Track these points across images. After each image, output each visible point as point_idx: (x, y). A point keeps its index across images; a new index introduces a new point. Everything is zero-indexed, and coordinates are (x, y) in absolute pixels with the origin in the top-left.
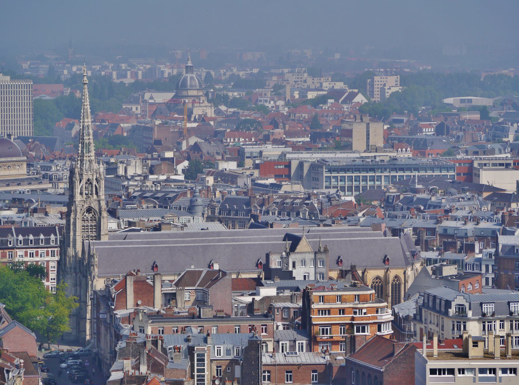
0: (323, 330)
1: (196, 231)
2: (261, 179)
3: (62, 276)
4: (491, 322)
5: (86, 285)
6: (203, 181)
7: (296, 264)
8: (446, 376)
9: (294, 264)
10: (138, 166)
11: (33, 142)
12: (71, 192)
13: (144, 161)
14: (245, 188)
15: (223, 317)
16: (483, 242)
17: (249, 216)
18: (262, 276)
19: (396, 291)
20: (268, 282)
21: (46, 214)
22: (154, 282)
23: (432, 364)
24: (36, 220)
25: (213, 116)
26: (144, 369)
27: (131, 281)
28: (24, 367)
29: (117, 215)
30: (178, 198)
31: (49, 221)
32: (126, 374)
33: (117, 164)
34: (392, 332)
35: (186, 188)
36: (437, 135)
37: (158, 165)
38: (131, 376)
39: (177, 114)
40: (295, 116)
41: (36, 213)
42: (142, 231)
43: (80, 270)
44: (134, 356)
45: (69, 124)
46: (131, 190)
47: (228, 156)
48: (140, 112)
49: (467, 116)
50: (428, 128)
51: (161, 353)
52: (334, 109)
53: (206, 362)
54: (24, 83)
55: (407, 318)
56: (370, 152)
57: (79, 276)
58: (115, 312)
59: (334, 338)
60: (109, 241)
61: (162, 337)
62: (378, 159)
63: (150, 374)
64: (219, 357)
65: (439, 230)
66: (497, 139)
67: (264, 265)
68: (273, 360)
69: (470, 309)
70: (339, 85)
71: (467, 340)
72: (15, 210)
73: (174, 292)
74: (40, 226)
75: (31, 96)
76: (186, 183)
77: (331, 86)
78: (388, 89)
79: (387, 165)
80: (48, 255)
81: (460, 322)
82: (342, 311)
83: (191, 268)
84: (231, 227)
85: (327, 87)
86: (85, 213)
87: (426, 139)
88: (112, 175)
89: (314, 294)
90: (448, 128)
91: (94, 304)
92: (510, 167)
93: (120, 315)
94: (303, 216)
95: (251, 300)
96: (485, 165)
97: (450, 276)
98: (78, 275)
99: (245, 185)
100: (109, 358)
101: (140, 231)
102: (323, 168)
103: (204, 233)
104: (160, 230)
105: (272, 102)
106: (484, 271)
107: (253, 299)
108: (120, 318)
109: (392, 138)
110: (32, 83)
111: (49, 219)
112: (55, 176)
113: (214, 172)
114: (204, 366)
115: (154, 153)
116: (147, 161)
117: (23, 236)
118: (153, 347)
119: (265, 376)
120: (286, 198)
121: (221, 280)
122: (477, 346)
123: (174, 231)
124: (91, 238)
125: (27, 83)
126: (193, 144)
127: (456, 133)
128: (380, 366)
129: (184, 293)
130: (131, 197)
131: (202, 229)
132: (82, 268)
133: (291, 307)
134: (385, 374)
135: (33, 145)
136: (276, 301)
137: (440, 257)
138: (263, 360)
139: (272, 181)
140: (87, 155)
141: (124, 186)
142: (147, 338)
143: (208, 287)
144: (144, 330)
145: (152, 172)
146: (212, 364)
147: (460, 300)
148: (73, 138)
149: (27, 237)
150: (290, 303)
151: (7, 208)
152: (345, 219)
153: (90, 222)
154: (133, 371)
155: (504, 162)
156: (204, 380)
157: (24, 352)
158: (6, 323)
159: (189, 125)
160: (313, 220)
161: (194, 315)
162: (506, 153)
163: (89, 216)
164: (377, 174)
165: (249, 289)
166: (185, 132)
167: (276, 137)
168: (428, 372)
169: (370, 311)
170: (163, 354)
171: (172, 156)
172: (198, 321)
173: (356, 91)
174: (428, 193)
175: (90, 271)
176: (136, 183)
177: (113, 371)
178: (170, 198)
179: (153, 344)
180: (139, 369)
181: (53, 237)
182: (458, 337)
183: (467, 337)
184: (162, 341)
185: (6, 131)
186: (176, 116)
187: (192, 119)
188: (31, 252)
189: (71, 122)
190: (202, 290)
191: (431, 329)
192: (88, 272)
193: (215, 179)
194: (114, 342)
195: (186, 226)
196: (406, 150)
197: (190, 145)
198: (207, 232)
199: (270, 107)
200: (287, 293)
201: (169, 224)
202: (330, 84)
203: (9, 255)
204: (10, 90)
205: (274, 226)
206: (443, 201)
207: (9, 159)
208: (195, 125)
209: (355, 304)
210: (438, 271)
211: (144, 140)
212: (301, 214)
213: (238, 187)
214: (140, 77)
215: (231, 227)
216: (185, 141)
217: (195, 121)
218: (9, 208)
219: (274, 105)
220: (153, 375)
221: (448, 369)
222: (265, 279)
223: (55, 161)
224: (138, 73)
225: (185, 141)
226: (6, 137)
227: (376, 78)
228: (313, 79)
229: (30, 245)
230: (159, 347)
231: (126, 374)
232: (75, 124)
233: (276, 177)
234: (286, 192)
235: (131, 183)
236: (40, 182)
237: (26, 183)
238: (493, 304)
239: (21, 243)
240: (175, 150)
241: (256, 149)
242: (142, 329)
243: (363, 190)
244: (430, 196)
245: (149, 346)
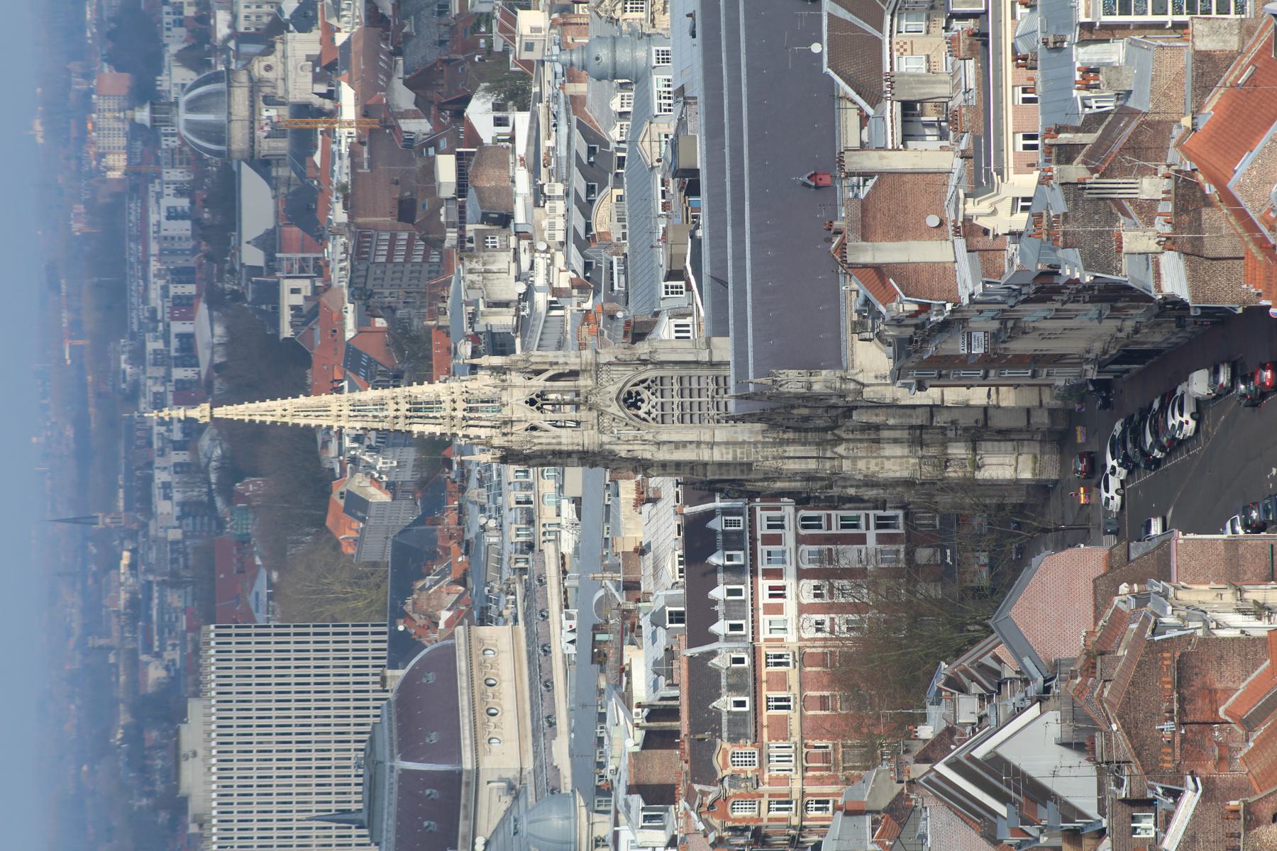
5: (877, 407)
6: (532, 44)
10: (484, 264)
12: (569, 460)
13: (469, 245)
21: (642, 551)
25: (316, 34)
26: (1151, 187)
27: (865, 250)
28: (1142, 581)
30: (591, 121)
31: (668, 541)
32: (1169, 243)
33: (477, 334)
35: (555, 97)
38: (1176, 227)
39: (312, 155)
41: (639, 583)
42: (699, 233)
43: (825, 430)
44: (1112, 218)
45: (347, 510)
46: (563, 281)
51: (1100, 132)
57: (847, 431)
58: (966, 301)
60: (731, 334)
63: (1169, 166)
72: (630, 653)
74: (681, 571)
76: (541, 101)
83: (821, 53)
86: (641, 413)
93: (974, 285)
98: (844, 436)
100: (1118, 323)
101: (700, 240)
110: (212, 627)
111: (660, 540)
112: (518, 536)
115: (442, 219)
116: (469, 234)
117: (716, 620)
118: (1080, 158)
123: (697, 126)
124: (721, 391)
125: (213, 643)
126: (412, 95)
130: (587, 278)
131: (694, 36)
141: (551, 306)
144: (1024, 199)
145: (505, 220)
148: (394, 499)
151: (625, 679)
154: (1159, 221)
158: (1002, 651)
161: (975, 35)
163: (650, 402)
170: (1103, 127)
172: (998, 21)
175: (831, 395)
176: (541, 263)
177: (1158, 286)
179: (1069, 161)
181: (717, 524)
184: (1059, 130)
185: (371, 695)
186: (317, 158)
187: (328, 105)
188: (767, 592)
189: (342, 502)
190: (892, 15)
194: (1064, 303)
197: (414, 107)
198: (709, 179)
201: (674, 145)
203: (777, 708)
208: (348, 95)
216: (401, 122)
217: (332, 95)
218: (624, 671)
220: (1173, 155)
223: (470, 536)
224: (177, 297)
225: (401, 122)
229: (747, 630)
231: (1169, 243)
232: (348, 491)
235: (540, 280)
236: (540, 581)
237: (538, 627)
239: (739, 627)
240: (431, 151)
245: (1076, 171)
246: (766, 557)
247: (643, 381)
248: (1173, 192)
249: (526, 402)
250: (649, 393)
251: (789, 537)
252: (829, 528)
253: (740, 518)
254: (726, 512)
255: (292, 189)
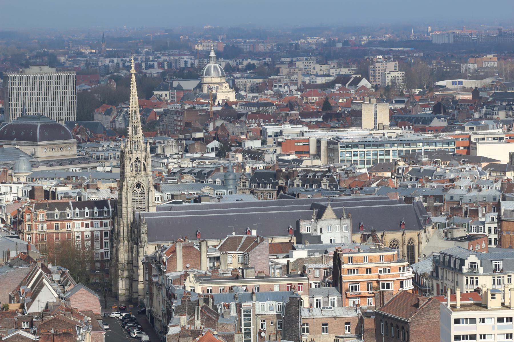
0: (352, 287)
1: (233, 202)
2: (284, 155)
3: (116, 243)
4: (500, 277)
7: (323, 230)
8: (469, 324)
9: (321, 229)
11: (79, 126)
13: (179, 141)
14: (271, 163)
15: (264, 277)
16: (485, 207)
17: (276, 188)
18: (294, 240)
19: (411, 251)
20: (300, 246)
21: (98, 189)
22: (200, 248)
23: (455, 315)
24: (90, 195)
25: (235, 100)
26: (198, 323)
30: (213, 173)
32: (183, 329)
33: (155, 144)
34: (413, 287)
35: (219, 164)
36: (435, 114)
37: (191, 144)
40: (307, 100)
41: (89, 188)
42: (184, 203)
46: (170, 167)
47: (251, 136)
49: (460, 97)
50: (427, 107)
52: (342, 92)
53: (252, 317)
54: (69, 74)
55: (424, 276)
56: (378, 130)
58: (167, 275)
59: (362, 294)
61: (213, 296)
62: (386, 136)
63: (203, 328)
64: (263, 313)
65: (447, 197)
66: (488, 116)
67: (295, 231)
68: (310, 314)
69: (481, 266)
70: (344, 71)
71: (486, 293)
72: (70, 186)
73: (218, 255)
74: (92, 200)
75: (74, 85)
77: (337, 72)
78: (388, 74)
79: (394, 141)
81: (473, 278)
82: (368, 271)
84: (260, 198)
85: (333, 73)
86: (135, 188)
87: (425, 118)
89: (344, 255)
90: (444, 107)
91: (146, 268)
92: (503, 141)
94: (324, 187)
95: (286, 262)
96: (483, 139)
97: (460, 237)
99: (272, 161)
100: (161, 316)
101: (182, 203)
102: (338, 145)
103: (238, 203)
104: (200, 202)
105: (286, 87)
106: (487, 233)
107: (288, 261)
108: (171, 280)
109: (395, 117)
114: (250, 321)
116: (182, 142)
117: (79, 209)
118: (205, 304)
119: (304, 328)
120: (309, 171)
121: (260, 245)
122: (494, 298)
127: (452, 111)
128: (406, 318)
129: (227, 257)
132: (133, 236)
133: (322, 267)
134: (411, 325)
135: (79, 129)
136: (308, 263)
137: (448, 221)
138: (302, 315)
139: (293, 157)
140: (136, 136)
141: (163, 164)
142: (200, 297)
143: (248, 251)
145: (186, 151)
146: (257, 318)
147: (473, 258)
149: (83, 209)
150: (321, 264)
152: (362, 189)
154: (189, 326)
155: (498, 136)
156: (250, 333)
157: (90, 311)
158: (72, 286)
159: (214, 109)
160: (334, 190)
162: (498, 128)
164: (386, 149)
165: (282, 252)
166: (212, 115)
167: (292, 118)
168: (453, 321)
169: (393, 269)
173: (360, 76)
174: (434, 164)
177: (171, 326)
178: (205, 174)
179: (204, 302)
181: (105, 209)
182: (473, 290)
183: (486, 291)
184: (213, 299)
187: (216, 103)
188: (87, 223)
189: (109, 108)
191: (447, 284)
192: (139, 240)
193: (244, 156)
194: (166, 301)
195: (222, 198)
196: (409, 127)
199: (284, 91)
200: (317, 255)
202: (336, 70)
205: (300, 196)
206: (447, 171)
207: (61, 141)
209: (380, 264)
210: (450, 233)
211: (175, 123)
212: (322, 185)
213: (264, 162)
214: (166, 67)
215: (260, 198)
216: (212, 123)
218: (65, 185)
219: (288, 90)
220: (207, 329)
221: (470, 319)
222: (296, 244)
227: (377, 65)
228: (321, 66)
230: (211, 304)
233: (297, 153)
234: (307, 166)
235: (170, 160)
238: (502, 261)
239: (77, 216)
240: (204, 131)
241: (277, 128)
243: (373, 163)
244: (435, 167)
245: (202, 303)
247: (144, 189)
252: (105, 239)
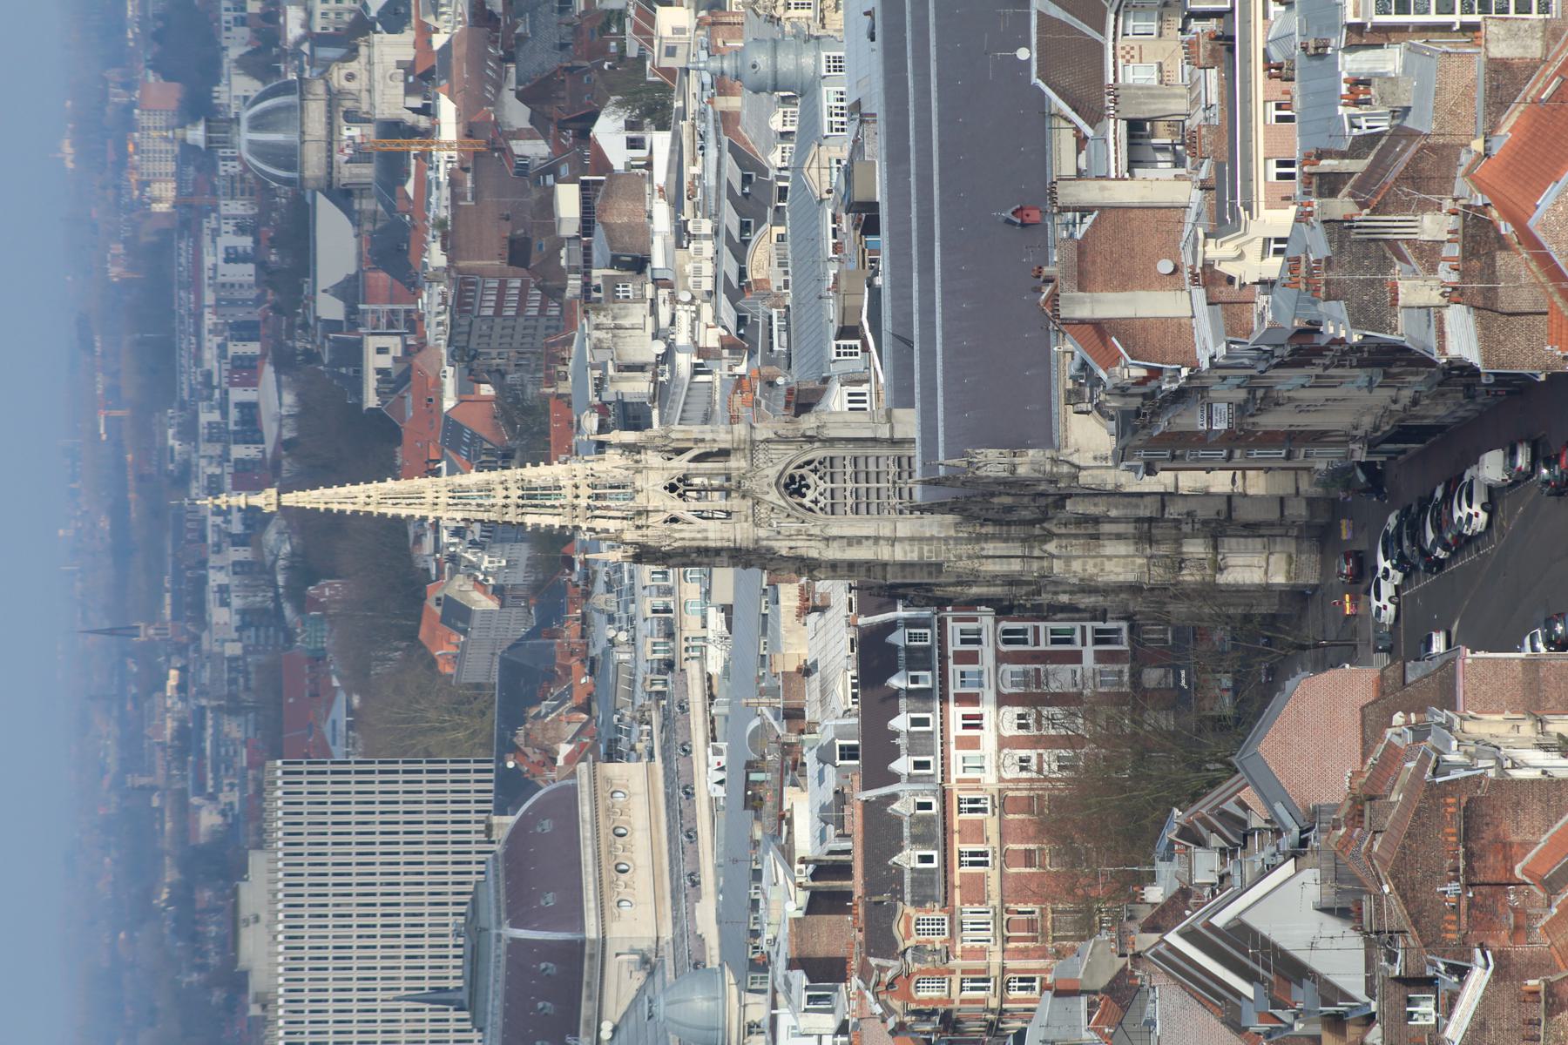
3: (1056, 593)
5: (1095, 495)
6: (674, 49)
12: (718, 559)
13: (595, 295)
22: (1085, 211)
25: (409, 35)
27: (1082, 302)
28: (1421, 710)
29: (811, 386)
30: (746, 143)
31: (838, 659)
32: (1455, 295)
33: (605, 404)
35: (702, 114)
37: (611, 240)
38: (1464, 274)
39: (403, 183)
42: (878, 281)
43: (1032, 523)
44: (1384, 265)
45: (445, 619)
46: (711, 339)
48: (397, 339)
51: (1371, 157)
54: (279, 793)
58: (1205, 365)
60: (917, 404)
63: (1455, 200)
72: (790, 794)
74: (854, 696)
80: (974, 743)
83: (1029, 60)
88: (650, 416)
98: (1056, 530)
100: (1392, 392)
101: (879, 290)
110: (279, 763)
111: (829, 658)
112: (654, 652)
113: (640, 12)
115: (563, 263)
116: (596, 281)
117: (895, 755)
118: (1346, 190)
123: (876, 150)
125: (280, 783)
126: (527, 111)
129: (1129, 87)
130: (741, 336)
132: (1026, 514)
135: (529, 751)
141: (697, 370)
144: (1278, 241)
145: (639, 264)
148: (502, 606)
151: (785, 828)
153: (838, 485)
154: (1443, 268)
157: (1363, 717)
158: (1248, 795)
163: (817, 487)
170: (1375, 151)
171: (576, 187)
172: (1246, 21)
175: (1039, 481)
177: (1442, 347)
178: (746, 180)
179: (1333, 193)
180: (1437, 244)
181: (898, 638)
184: (1321, 155)
186: (410, 187)
187: (423, 122)
188: (961, 722)
189: (438, 610)
194: (1326, 367)
197: (529, 126)
201: (848, 173)
204: (305, 808)
207: (586, 832)
208: (447, 110)
214: (253, 348)
216: (513, 143)
217: (428, 110)
218: (784, 819)
220: (1461, 186)
225: (513, 143)
226: (495, 847)
235: (682, 338)
236: (681, 707)
237: (679, 764)
239: (926, 765)
242: (1273, 246)
245: (1342, 206)
246: (958, 679)
247: (809, 463)
248: (1460, 232)
249: (665, 488)
250: (816, 478)
251: (987, 654)
252: (1037, 643)
253: (928, 631)
254: (910, 623)
255: (379, 225)
